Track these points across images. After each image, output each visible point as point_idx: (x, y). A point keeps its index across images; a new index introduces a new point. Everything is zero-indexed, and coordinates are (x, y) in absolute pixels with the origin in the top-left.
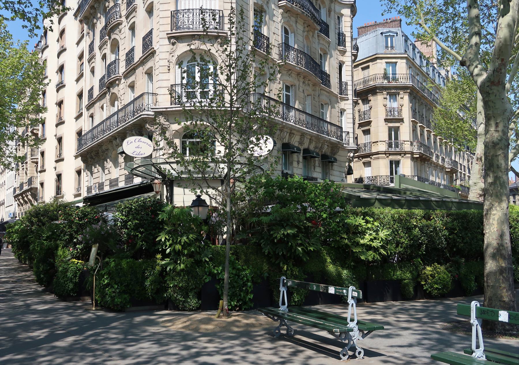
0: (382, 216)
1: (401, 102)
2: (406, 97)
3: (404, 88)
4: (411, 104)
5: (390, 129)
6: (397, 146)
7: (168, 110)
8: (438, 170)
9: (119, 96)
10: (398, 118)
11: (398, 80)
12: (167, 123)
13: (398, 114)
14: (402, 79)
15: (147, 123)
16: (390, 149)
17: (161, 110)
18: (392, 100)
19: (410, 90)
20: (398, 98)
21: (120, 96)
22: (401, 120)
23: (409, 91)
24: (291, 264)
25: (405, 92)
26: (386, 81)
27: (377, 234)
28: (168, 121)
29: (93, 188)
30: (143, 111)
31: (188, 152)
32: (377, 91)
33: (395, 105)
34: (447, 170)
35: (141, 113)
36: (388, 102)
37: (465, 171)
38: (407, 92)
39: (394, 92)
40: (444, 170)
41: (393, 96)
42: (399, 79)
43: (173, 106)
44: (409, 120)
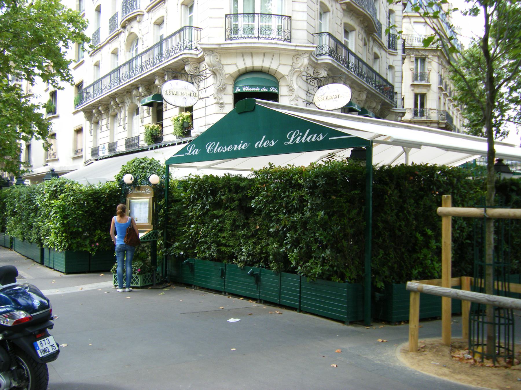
5: (416, 95)
6: (422, 114)
9: (139, 36)
16: (415, 117)
21: (142, 37)
29: (100, 149)
30: (184, 49)
35: (182, 52)
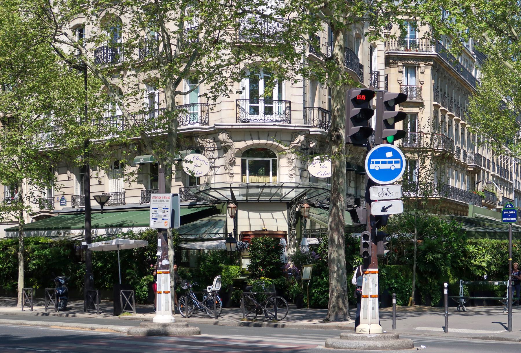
0: (486, 245)
1: (421, 78)
2: (428, 72)
3: (426, 59)
4: (433, 81)
7: (234, 127)
8: (459, 170)
10: (417, 101)
11: (419, 47)
12: (231, 141)
13: (416, 94)
14: (423, 46)
15: (198, 137)
17: (226, 127)
18: (409, 74)
19: (435, 62)
20: (418, 72)
22: (421, 105)
23: (432, 63)
24: (434, 278)
25: (427, 65)
26: (403, 48)
27: (484, 258)
28: (231, 138)
31: (247, 171)
32: (391, 61)
33: (412, 82)
34: (469, 169)
36: (403, 78)
37: (489, 168)
38: (430, 65)
39: (412, 64)
40: (465, 169)
41: (411, 69)
42: (420, 46)
43: (238, 123)
44: (431, 103)
